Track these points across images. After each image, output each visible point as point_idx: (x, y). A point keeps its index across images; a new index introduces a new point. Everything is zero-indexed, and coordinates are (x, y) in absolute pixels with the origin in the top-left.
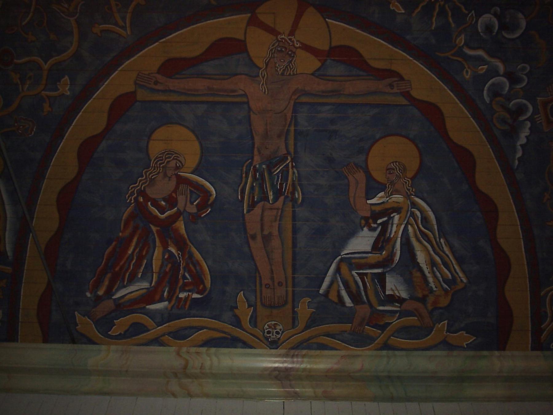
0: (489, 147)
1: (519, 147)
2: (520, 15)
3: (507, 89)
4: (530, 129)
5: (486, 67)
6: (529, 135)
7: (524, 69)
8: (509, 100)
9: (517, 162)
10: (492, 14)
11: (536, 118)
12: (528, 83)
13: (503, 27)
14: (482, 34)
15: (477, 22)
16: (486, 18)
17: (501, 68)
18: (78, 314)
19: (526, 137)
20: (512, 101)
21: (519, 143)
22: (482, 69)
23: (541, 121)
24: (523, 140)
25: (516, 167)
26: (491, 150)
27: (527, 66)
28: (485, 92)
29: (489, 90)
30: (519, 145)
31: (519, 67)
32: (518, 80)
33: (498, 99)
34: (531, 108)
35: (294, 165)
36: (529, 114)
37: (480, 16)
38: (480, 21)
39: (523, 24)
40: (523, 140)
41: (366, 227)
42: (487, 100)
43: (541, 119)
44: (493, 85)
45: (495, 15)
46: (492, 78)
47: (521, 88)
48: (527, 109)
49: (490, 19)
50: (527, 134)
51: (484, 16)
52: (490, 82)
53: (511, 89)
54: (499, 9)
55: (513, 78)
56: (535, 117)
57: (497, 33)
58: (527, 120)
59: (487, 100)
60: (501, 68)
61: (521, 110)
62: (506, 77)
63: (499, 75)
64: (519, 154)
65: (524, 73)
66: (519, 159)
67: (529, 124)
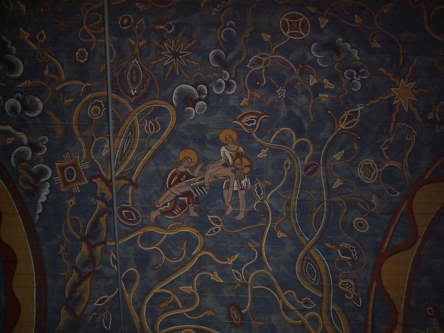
0: (14, 203)
1: (40, 204)
2: (38, 100)
3: (30, 155)
4: (50, 189)
5: (13, 138)
6: (49, 194)
7: (44, 140)
8: (33, 165)
9: (37, 217)
10: (16, 99)
11: (55, 179)
12: (47, 150)
13: (25, 108)
14: (8, 113)
15: (4, 104)
16: (12, 101)
17: (25, 139)
18: (336, 129)
19: (47, 196)
20: (34, 166)
21: (40, 201)
22: (10, 140)
23: (59, 182)
24: (43, 198)
25: (36, 222)
26: (15, 206)
27: (46, 138)
28: (12, 158)
29: (15, 157)
30: (40, 202)
31: (39, 139)
32: (38, 149)
33: (24, 164)
34: (50, 172)
35: (315, 166)
36: (49, 176)
37: (6, 101)
38: (7, 103)
39: (41, 105)
40: (43, 198)
41: (239, 159)
42: (14, 164)
43: (59, 181)
44: (19, 152)
45: (18, 99)
46: (18, 147)
47: (42, 155)
48: (47, 172)
49: (15, 103)
50: (47, 193)
51: (9, 100)
52: (16, 151)
53: (33, 155)
54: (20, 95)
55: (35, 148)
56: (54, 179)
57: (21, 113)
58: (47, 181)
59: (14, 164)
60: (25, 139)
61: (42, 173)
62: (29, 147)
63: (24, 145)
64: (40, 210)
65: (43, 143)
66: (40, 214)
67: (48, 185)
